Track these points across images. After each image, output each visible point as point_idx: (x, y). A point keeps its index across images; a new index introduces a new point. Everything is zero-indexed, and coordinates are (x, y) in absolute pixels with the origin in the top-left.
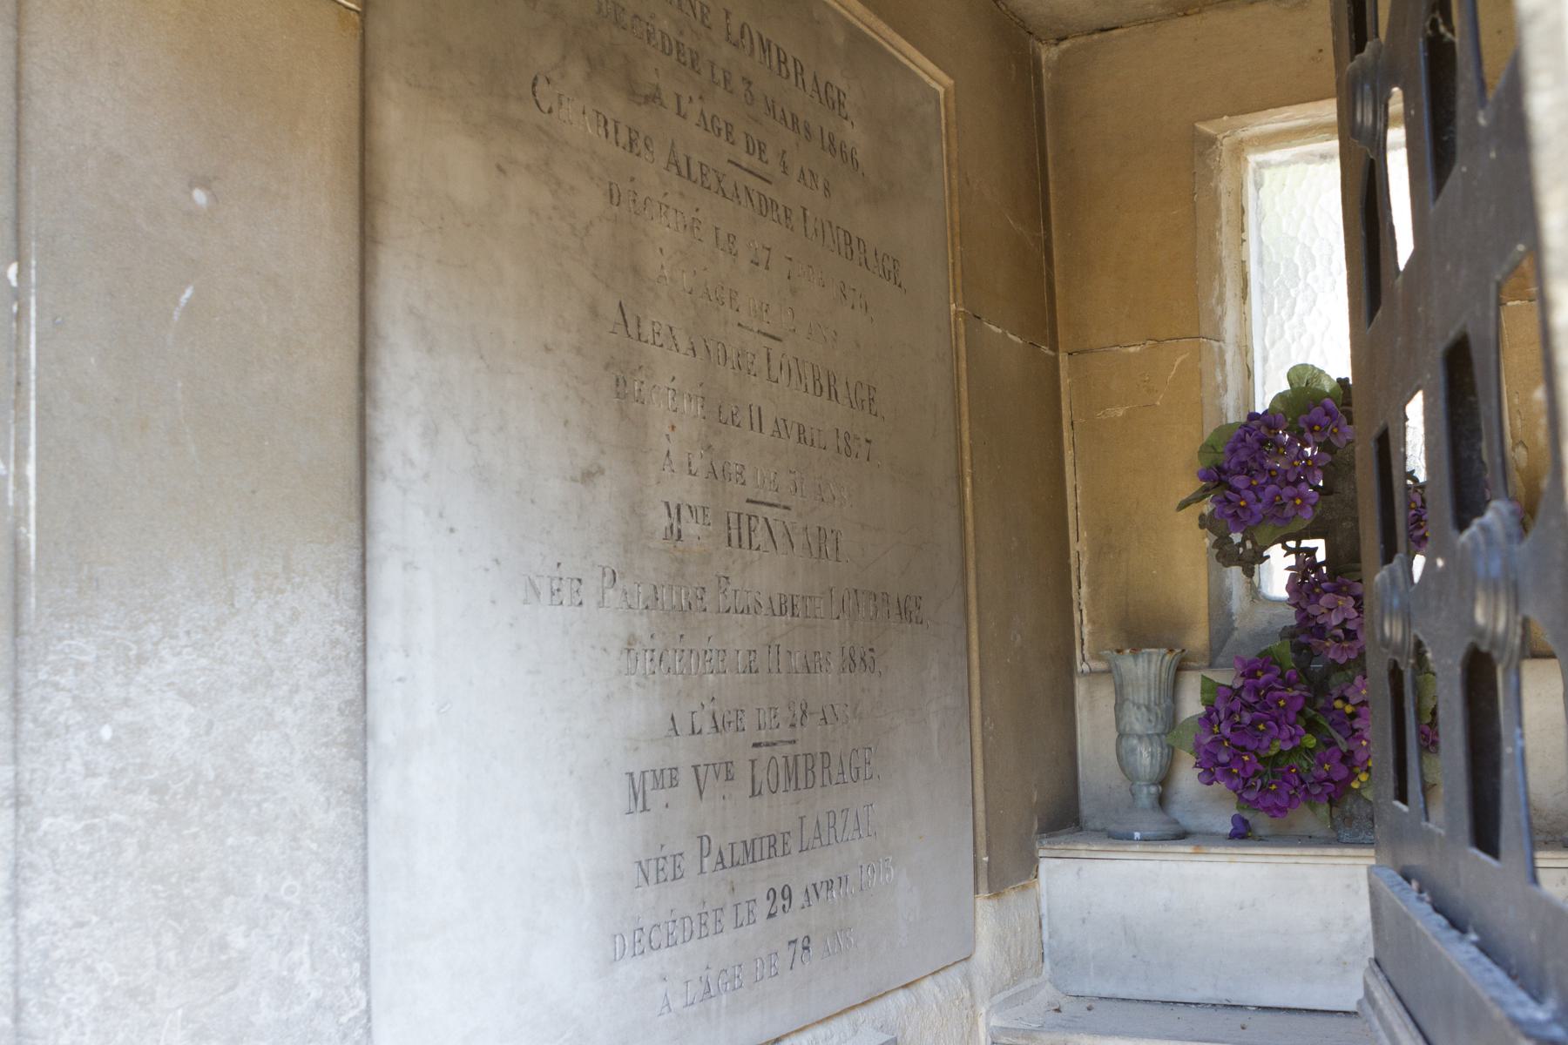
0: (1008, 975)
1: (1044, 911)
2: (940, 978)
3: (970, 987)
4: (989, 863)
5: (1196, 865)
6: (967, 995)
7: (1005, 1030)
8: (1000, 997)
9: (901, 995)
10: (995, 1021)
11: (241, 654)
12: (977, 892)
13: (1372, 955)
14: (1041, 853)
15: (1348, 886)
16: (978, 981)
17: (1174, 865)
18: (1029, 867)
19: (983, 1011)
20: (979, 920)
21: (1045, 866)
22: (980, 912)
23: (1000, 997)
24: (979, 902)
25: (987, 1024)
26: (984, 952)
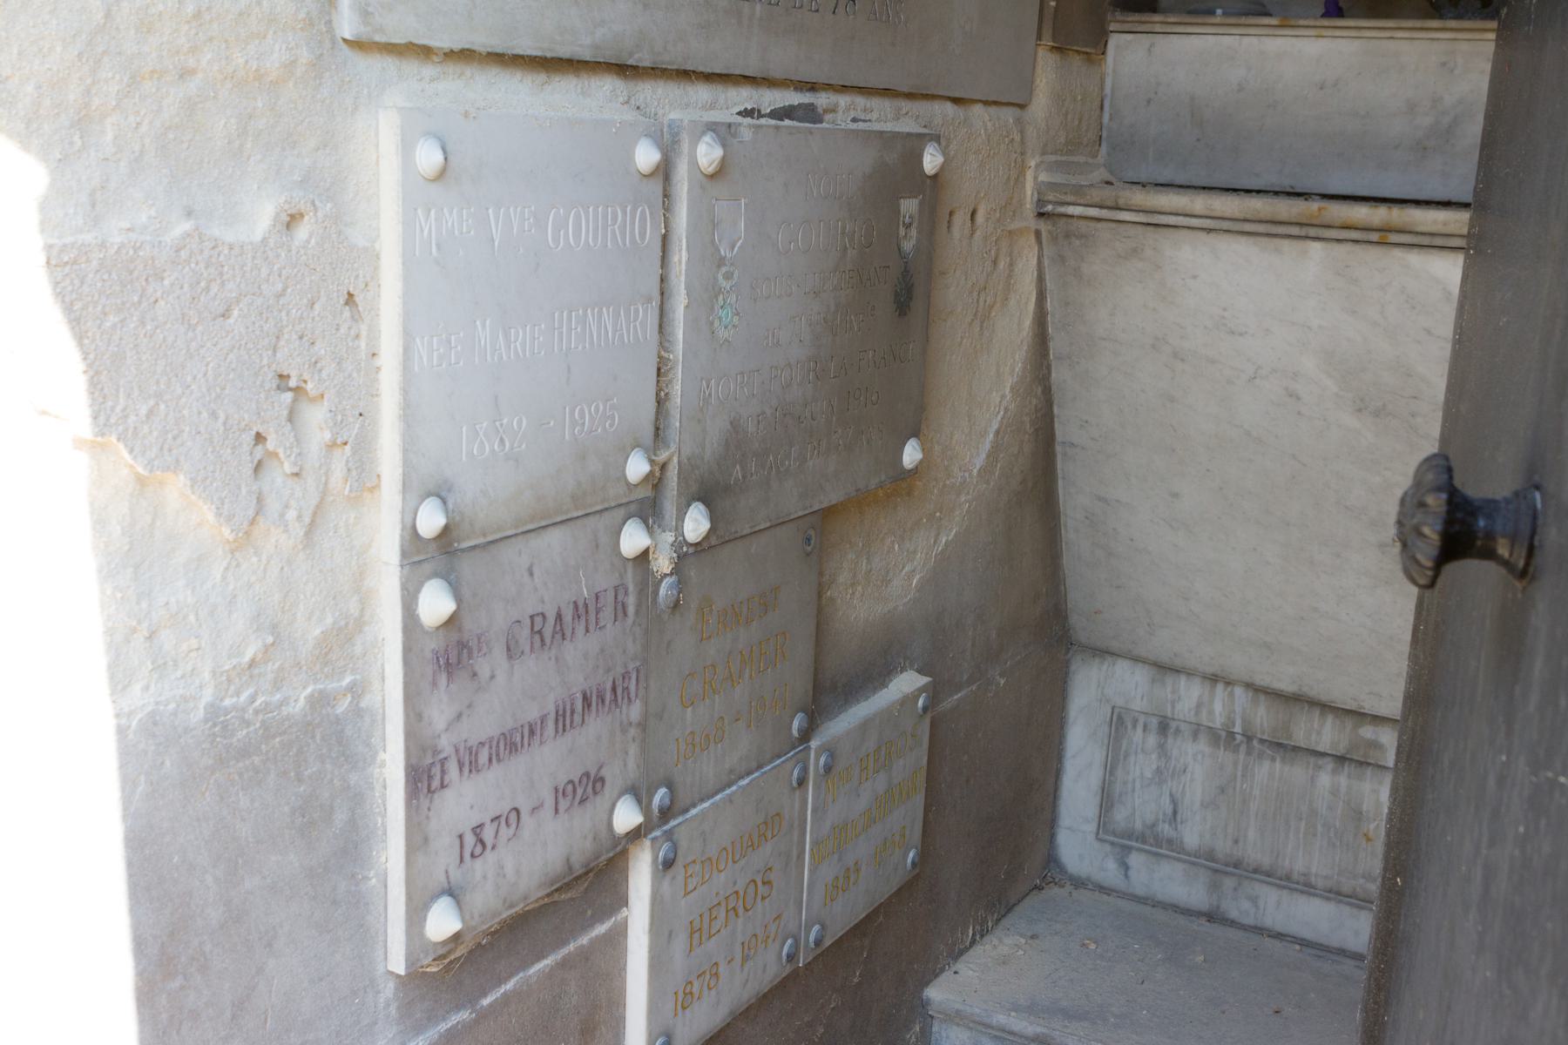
0: (1062, 140)
1: (1108, 90)
2: (993, 110)
3: (1022, 132)
4: (1056, 9)
5: (1279, 41)
6: (1017, 138)
7: (1053, 186)
8: (1053, 158)
9: (949, 107)
10: (1043, 177)
11: (278, 256)
12: (1039, 37)
13: (1432, 448)
14: (1109, 17)
15: (1444, 64)
16: (1031, 132)
17: (1254, 40)
18: (1098, 40)
19: (1033, 164)
20: (1039, 71)
21: (1114, 41)
22: (1040, 63)
23: (1053, 158)
24: (1041, 52)
25: (1036, 178)
26: (1040, 105)
